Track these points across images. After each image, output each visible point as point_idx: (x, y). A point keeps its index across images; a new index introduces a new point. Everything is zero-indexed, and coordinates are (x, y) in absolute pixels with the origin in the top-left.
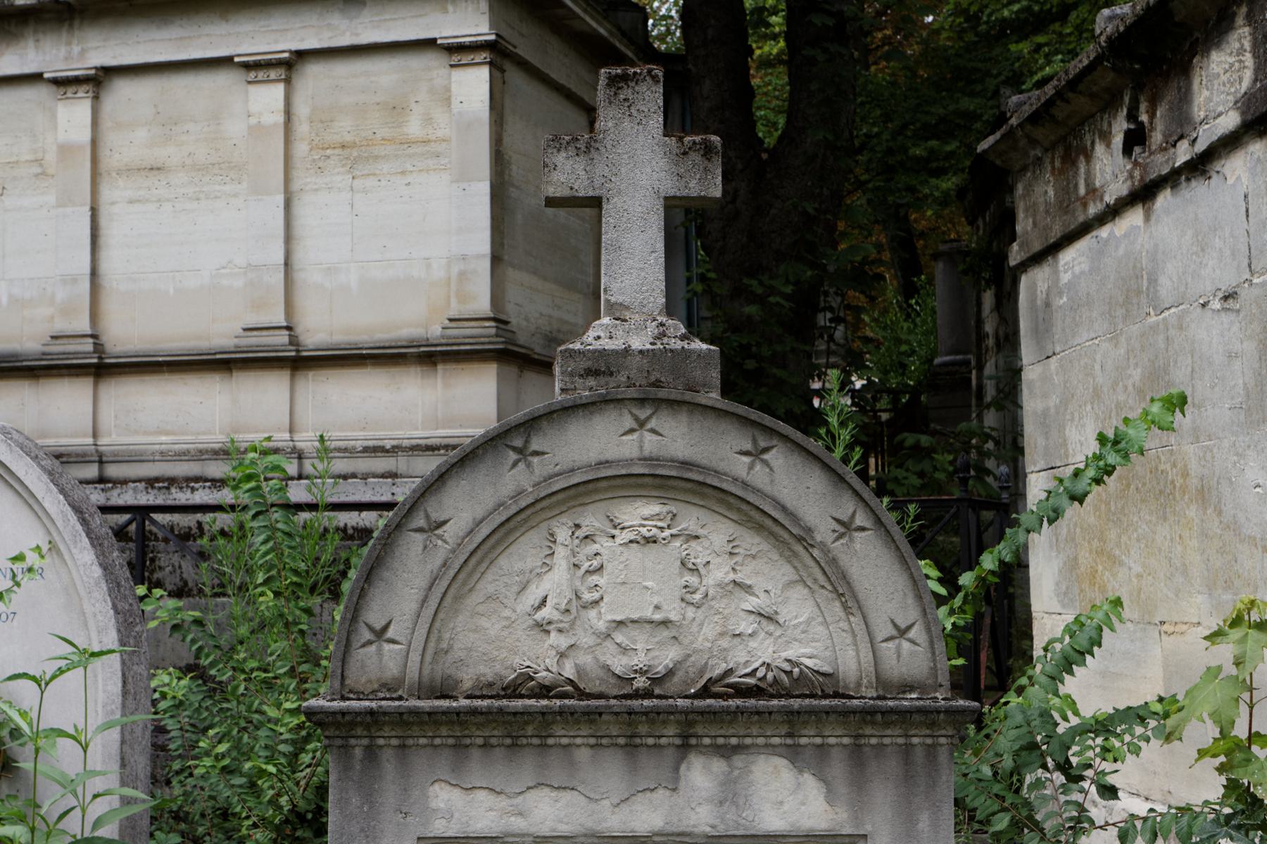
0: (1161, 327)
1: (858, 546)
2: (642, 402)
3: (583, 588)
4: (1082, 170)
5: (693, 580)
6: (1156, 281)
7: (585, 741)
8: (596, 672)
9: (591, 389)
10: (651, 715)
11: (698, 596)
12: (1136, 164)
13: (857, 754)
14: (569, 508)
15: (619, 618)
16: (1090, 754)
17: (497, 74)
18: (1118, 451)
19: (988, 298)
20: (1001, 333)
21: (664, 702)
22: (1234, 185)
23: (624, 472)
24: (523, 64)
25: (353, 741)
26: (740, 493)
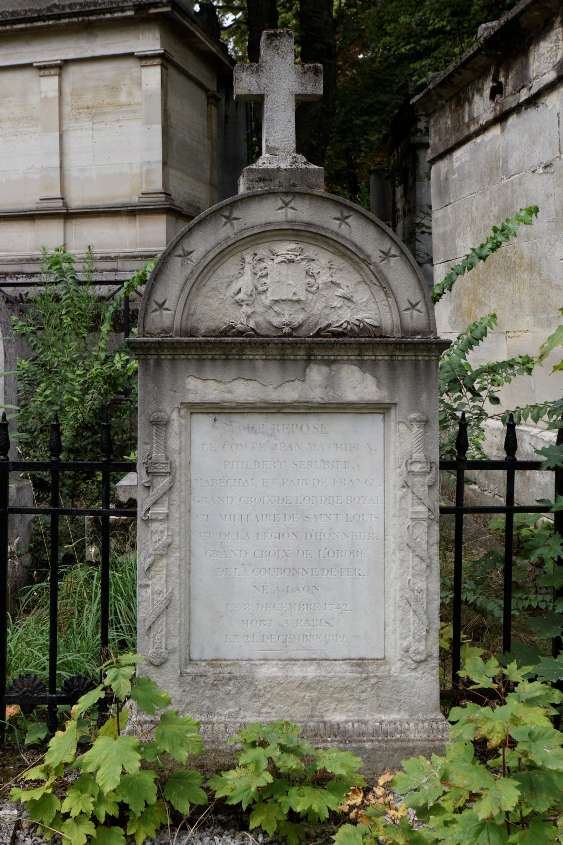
0: (510, 185)
1: (392, 264)
2: (287, 193)
3: (258, 285)
4: (467, 109)
5: (312, 281)
6: (507, 162)
7: (261, 357)
8: (264, 325)
9: (261, 188)
10: (293, 345)
11: (314, 289)
12: (497, 103)
13: (392, 365)
14: (251, 246)
15: (276, 299)
16: (486, 382)
17: (164, 70)
18: (504, 235)
19: (399, 191)
20: (406, 208)
21: (298, 339)
22: (551, 109)
23: (278, 228)
24: (177, 67)
25: (149, 357)
26: (335, 238)
